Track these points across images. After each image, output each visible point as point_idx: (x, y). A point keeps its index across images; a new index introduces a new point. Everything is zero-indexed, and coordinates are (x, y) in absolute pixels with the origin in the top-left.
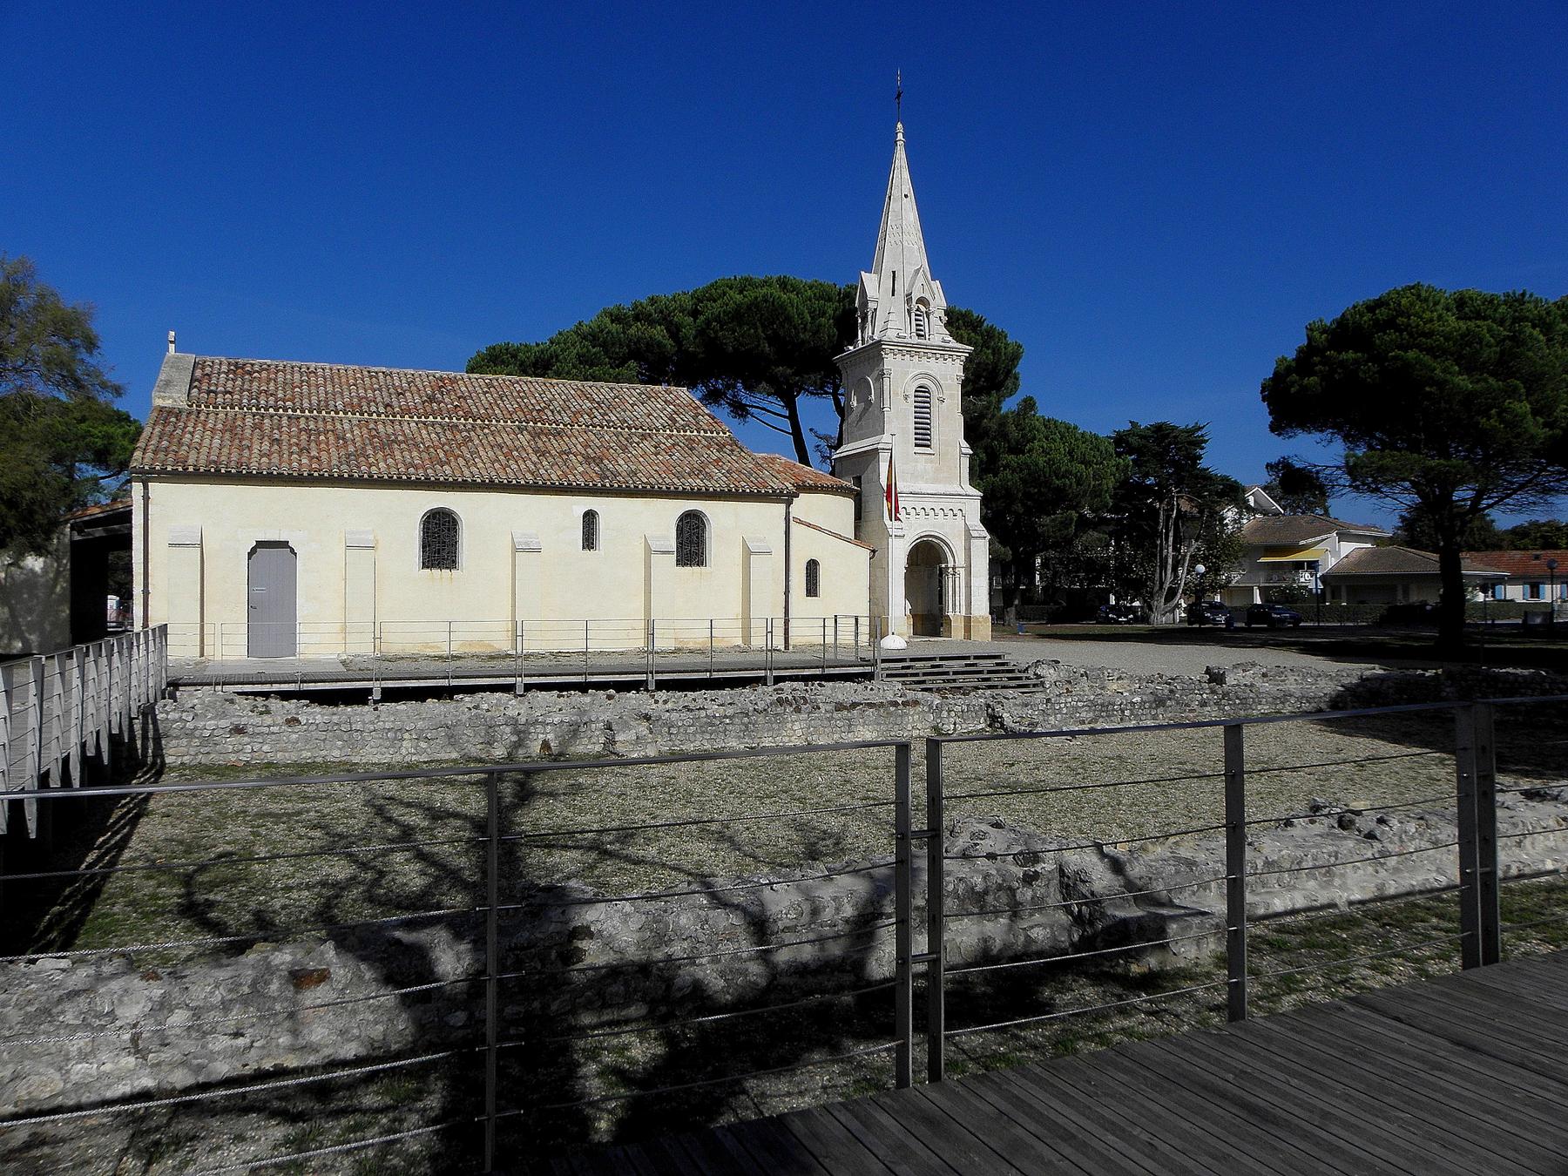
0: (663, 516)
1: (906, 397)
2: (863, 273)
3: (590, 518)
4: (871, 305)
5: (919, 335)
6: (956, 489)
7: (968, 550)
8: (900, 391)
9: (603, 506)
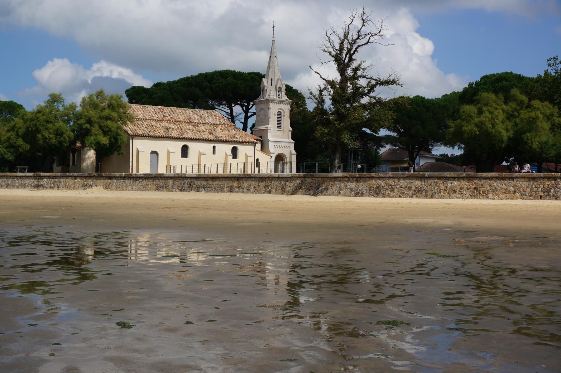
0: (228, 148)
1: (275, 115)
2: (263, 78)
3: (214, 147)
4: (266, 88)
5: (278, 97)
6: (287, 140)
7: (291, 158)
8: (274, 113)
9: (216, 145)
